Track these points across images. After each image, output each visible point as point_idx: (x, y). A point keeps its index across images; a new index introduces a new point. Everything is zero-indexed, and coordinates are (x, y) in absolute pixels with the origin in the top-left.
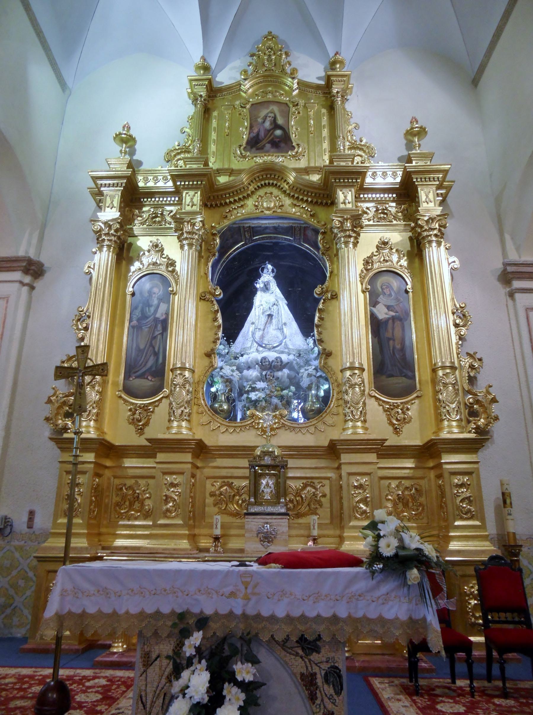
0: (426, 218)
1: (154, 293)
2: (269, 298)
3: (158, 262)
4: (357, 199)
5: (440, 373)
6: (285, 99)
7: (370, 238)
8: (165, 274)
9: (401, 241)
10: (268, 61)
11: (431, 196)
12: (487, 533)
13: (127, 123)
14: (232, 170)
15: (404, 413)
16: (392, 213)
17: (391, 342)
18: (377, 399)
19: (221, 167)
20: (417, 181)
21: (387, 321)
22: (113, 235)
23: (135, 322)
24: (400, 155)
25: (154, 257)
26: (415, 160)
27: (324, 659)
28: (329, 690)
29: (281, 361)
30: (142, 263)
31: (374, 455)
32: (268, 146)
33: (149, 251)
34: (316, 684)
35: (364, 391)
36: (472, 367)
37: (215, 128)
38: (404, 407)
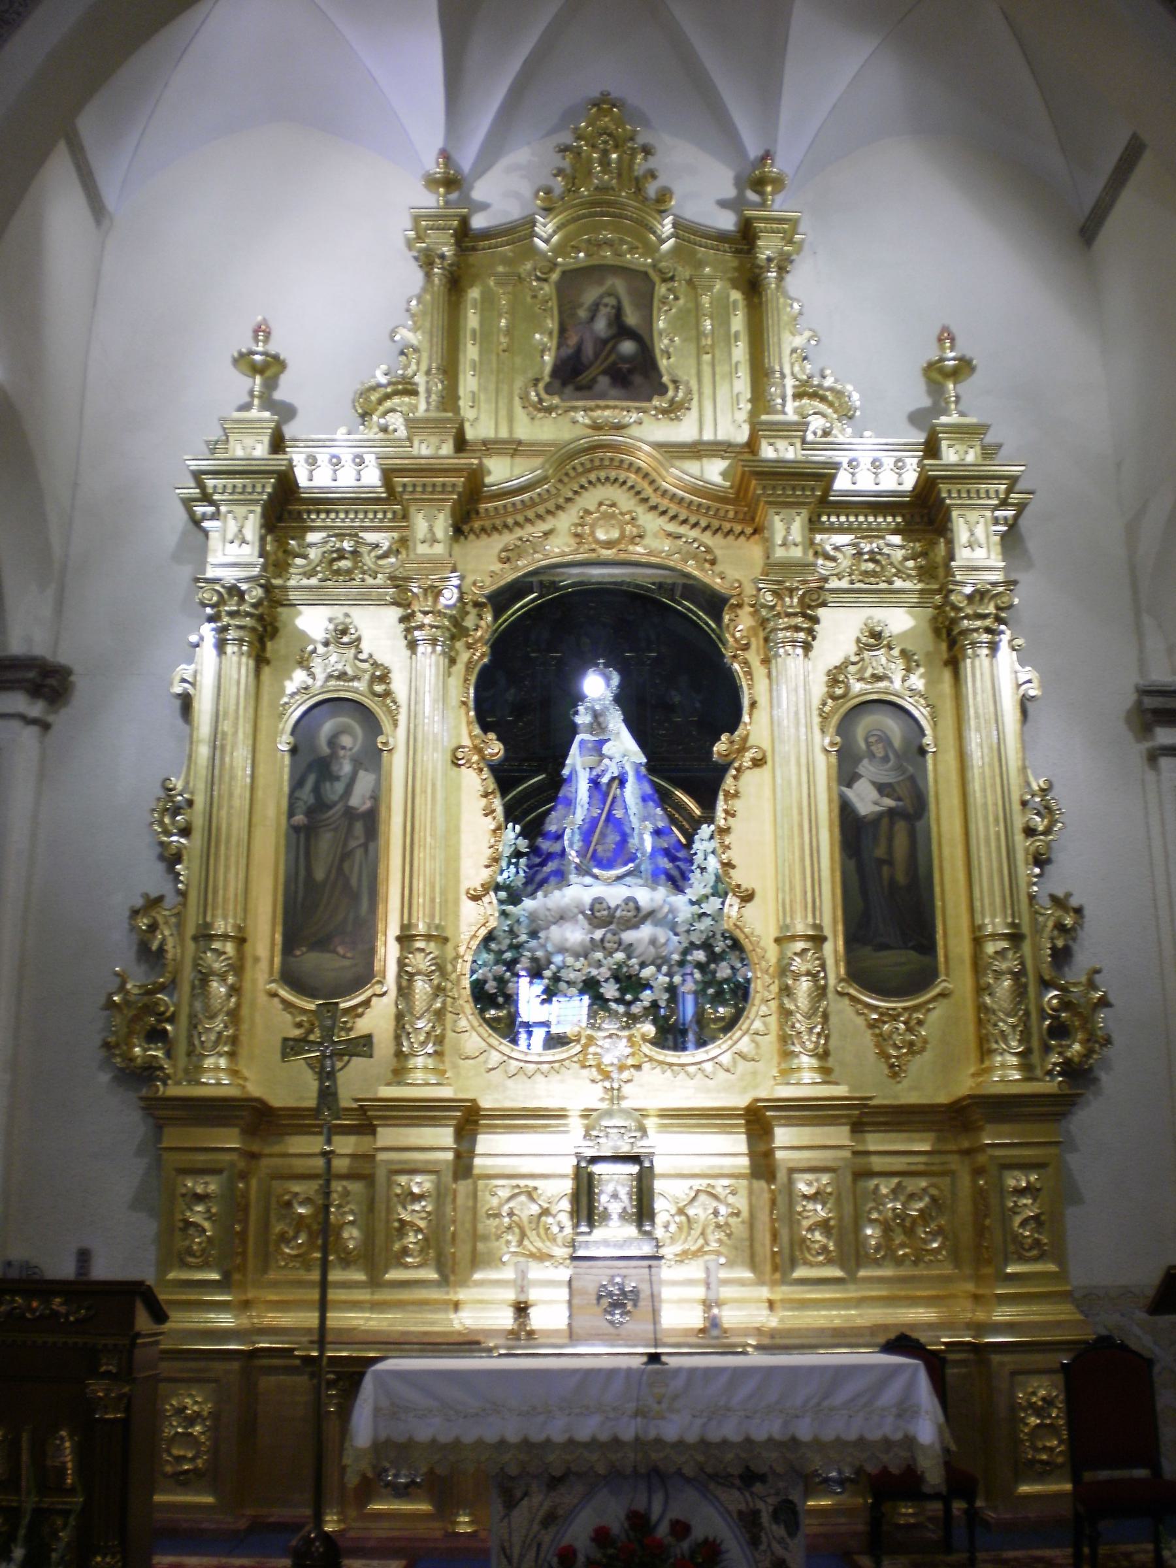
0: (968, 590)
1: (344, 748)
2: (606, 745)
3: (350, 671)
4: (814, 525)
5: (991, 948)
6: (638, 260)
7: (839, 630)
8: (367, 702)
9: (913, 629)
10: (601, 164)
11: (980, 531)
12: (1068, 1288)
13: (264, 319)
14: (520, 443)
15: (909, 1030)
16: (893, 559)
17: (885, 869)
18: (853, 999)
19: (491, 434)
20: (950, 498)
21: (877, 819)
22: (248, 614)
23: (300, 819)
24: (912, 408)
25: (336, 660)
26: (947, 439)
27: (772, 1491)
28: (780, 1531)
29: (638, 909)
30: (312, 675)
31: (846, 1130)
32: (604, 381)
33: (326, 644)
34: (760, 1524)
35: (825, 988)
36: (1060, 927)
37: (474, 331)
38: (910, 1018)
